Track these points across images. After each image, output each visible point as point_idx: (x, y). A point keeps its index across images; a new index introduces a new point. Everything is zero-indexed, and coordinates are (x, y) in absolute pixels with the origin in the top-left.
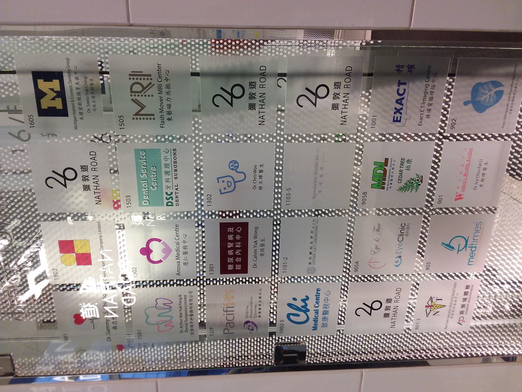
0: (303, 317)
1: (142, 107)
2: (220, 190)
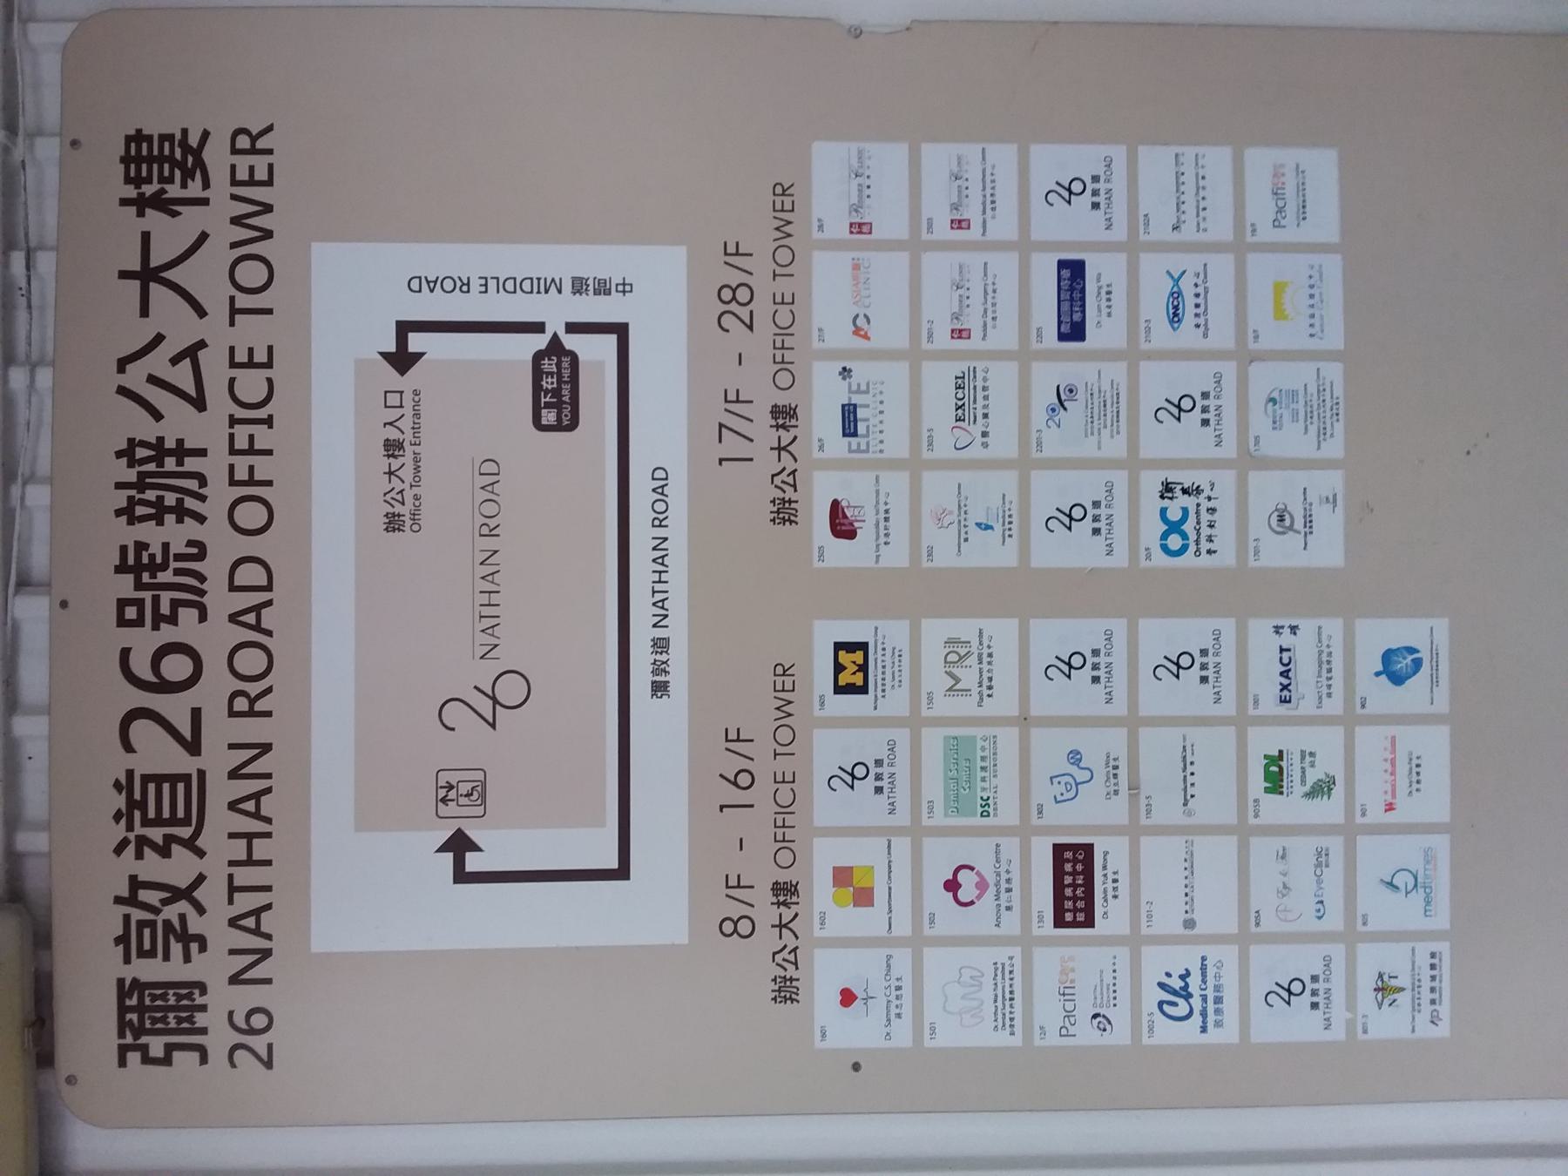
0: (1182, 1008)
1: (958, 680)
2: (232, 349)
